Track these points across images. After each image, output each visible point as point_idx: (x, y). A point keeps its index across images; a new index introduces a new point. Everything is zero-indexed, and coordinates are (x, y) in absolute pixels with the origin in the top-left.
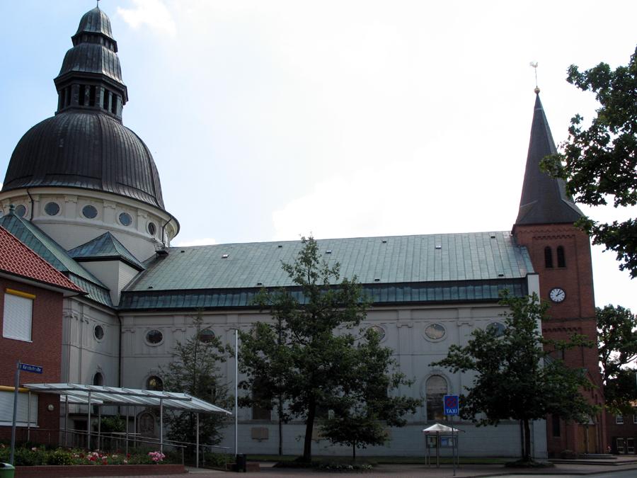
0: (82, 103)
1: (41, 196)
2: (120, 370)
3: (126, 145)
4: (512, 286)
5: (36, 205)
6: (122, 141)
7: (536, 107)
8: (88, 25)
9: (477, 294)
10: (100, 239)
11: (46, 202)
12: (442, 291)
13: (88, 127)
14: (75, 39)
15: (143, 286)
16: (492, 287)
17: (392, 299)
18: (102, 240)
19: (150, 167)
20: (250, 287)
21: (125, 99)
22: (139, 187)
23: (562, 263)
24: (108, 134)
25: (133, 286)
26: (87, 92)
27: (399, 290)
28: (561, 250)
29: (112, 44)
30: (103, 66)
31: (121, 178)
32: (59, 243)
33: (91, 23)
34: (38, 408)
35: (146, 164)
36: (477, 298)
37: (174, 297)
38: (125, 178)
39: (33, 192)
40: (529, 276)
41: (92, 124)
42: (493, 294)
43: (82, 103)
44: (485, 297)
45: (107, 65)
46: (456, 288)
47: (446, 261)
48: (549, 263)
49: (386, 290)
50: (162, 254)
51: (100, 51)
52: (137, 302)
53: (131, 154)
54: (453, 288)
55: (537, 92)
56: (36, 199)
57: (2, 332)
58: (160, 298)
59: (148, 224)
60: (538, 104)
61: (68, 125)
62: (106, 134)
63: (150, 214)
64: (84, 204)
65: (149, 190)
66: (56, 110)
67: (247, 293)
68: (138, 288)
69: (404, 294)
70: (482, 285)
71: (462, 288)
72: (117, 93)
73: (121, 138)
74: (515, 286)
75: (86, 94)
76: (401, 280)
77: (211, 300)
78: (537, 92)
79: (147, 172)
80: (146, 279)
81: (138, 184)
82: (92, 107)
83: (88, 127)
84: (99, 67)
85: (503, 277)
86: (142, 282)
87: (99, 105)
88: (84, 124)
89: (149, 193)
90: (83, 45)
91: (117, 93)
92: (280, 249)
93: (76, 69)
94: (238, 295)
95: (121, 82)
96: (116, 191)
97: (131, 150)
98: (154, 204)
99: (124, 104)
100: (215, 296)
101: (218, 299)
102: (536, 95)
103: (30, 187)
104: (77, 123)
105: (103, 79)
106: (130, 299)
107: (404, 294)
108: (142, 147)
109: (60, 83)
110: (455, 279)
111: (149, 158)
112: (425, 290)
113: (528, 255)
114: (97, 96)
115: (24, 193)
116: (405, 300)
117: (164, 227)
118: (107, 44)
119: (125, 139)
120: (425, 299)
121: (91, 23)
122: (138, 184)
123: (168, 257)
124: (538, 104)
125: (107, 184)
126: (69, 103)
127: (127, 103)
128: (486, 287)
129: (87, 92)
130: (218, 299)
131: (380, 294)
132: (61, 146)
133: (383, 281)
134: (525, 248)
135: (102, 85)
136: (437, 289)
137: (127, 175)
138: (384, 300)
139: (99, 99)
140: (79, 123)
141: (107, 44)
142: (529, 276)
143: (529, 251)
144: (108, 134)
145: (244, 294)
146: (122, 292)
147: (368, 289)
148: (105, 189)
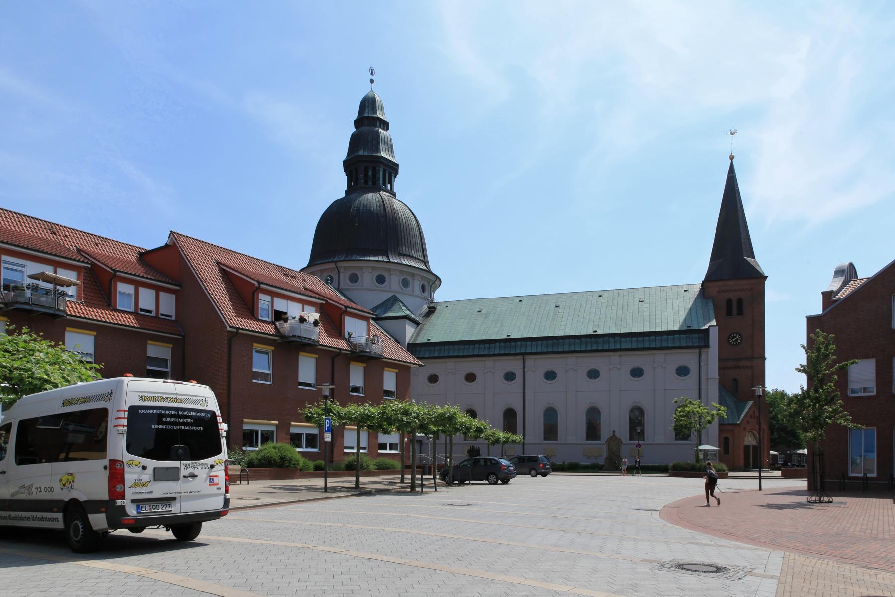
0: (366, 182)
1: (345, 268)
2: (524, 393)
3: (404, 220)
4: (697, 335)
5: (341, 275)
6: (400, 216)
7: (729, 173)
8: (367, 110)
9: (669, 342)
10: (389, 301)
11: (348, 273)
12: (644, 340)
13: (375, 206)
14: (357, 123)
15: (422, 339)
16: (681, 336)
17: (606, 347)
18: (391, 302)
19: (420, 236)
20: (501, 338)
21: (396, 172)
22: (414, 255)
23: (740, 312)
24: (390, 212)
25: (415, 339)
26: (370, 173)
27: (611, 339)
28: (740, 301)
29: (385, 125)
30: (381, 147)
31: (401, 248)
32: (351, 299)
33: (369, 107)
34: (161, 480)
35: (417, 233)
36: (669, 345)
37: (446, 347)
38: (404, 248)
39: (340, 265)
40: (710, 328)
41: (378, 204)
42: (682, 342)
43: (366, 182)
44: (676, 345)
45: (383, 146)
46: (654, 337)
47: (647, 314)
48: (729, 313)
49: (601, 339)
50: (432, 310)
51: (378, 133)
52: (420, 351)
53: (407, 227)
54: (651, 338)
55: (732, 158)
56: (342, 270)
57: (349, 382)
58: (436, 348)
59: (421, 284)
60: (732, 170)
61: (360, 205)
62: (389, 213)
63: (373, 268)
64: (376, 274)
65: (420, 256)
66: (346, 189)
67: (500, 343)
68: (419, 341)
69: (615, 342)
70: (662, 336)
71: (658, 338)
72: (392, 171)
73: (399, 213)
74: (700, 335)
75: (370, 174)
76: (613, 331)
77: (474, 349)
78: (732, 158)
79: (418, 241)
80: (423, 332)
81: (413, 252)
82: (376, 188)
83: (375, 206)
84: (378, 150)
85: (690, 329)
86: (421, 335)
87: (380, 183)
88: (372, 203)
89: (421, 259)
90: (365, 129)
91: (392, 171)
92: (521, 303)
93: (361, 153)
94: (493, 345)
95: (394, 161)
96: (399, 262)
97: (407, 223)
98: (424, 268)
99: (396, 177)
100: (477, 346)
101: (479, 348)
102: (730, 160)
103: (336, 262)
104: (367, 204)
105: (382, 160)
106: (414, 349)
107: (615, 342)
108: (414, 219)
109: (349, 166)
110: (653, 330)
111: (419, 230)
112: (630, 339)
113: (712, 307)
114: (378, 176)
115: (332, 265)
116: (616, 348)
117: (431, 286)
118: (382, 126)
119: (402, 214)
120: (630, 347)
121: (369, 107)
122: (413, 252)
123: (436, 311)
124: (732, 170)
125: (392, 253)
126: (356, 183)
127: (397, 176)
128: (677, 336)
129: (370, 173)
130: (479, 348)
131: (597, 343)
132: (357, 224)
133: (600, 332)
134: (711, 300)
135: (382, 166)
136: (639, 338)
137: (405, 245)
138: (600, 348)
139: (379, 178)
140: (368, 203)
141: (382, 126)
142: (710, 328)
143: (713, 303)
144: (390, 212)
145: (497, 344)
146: (408, 344)
147: (588, 339)
148: (392, 260)
